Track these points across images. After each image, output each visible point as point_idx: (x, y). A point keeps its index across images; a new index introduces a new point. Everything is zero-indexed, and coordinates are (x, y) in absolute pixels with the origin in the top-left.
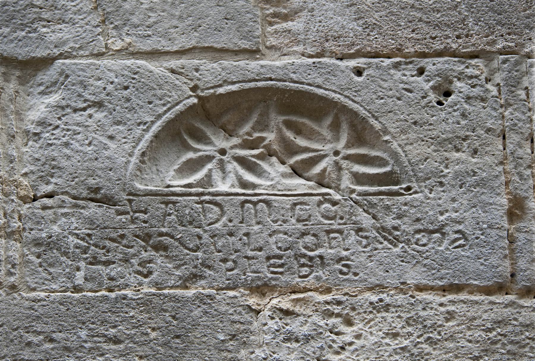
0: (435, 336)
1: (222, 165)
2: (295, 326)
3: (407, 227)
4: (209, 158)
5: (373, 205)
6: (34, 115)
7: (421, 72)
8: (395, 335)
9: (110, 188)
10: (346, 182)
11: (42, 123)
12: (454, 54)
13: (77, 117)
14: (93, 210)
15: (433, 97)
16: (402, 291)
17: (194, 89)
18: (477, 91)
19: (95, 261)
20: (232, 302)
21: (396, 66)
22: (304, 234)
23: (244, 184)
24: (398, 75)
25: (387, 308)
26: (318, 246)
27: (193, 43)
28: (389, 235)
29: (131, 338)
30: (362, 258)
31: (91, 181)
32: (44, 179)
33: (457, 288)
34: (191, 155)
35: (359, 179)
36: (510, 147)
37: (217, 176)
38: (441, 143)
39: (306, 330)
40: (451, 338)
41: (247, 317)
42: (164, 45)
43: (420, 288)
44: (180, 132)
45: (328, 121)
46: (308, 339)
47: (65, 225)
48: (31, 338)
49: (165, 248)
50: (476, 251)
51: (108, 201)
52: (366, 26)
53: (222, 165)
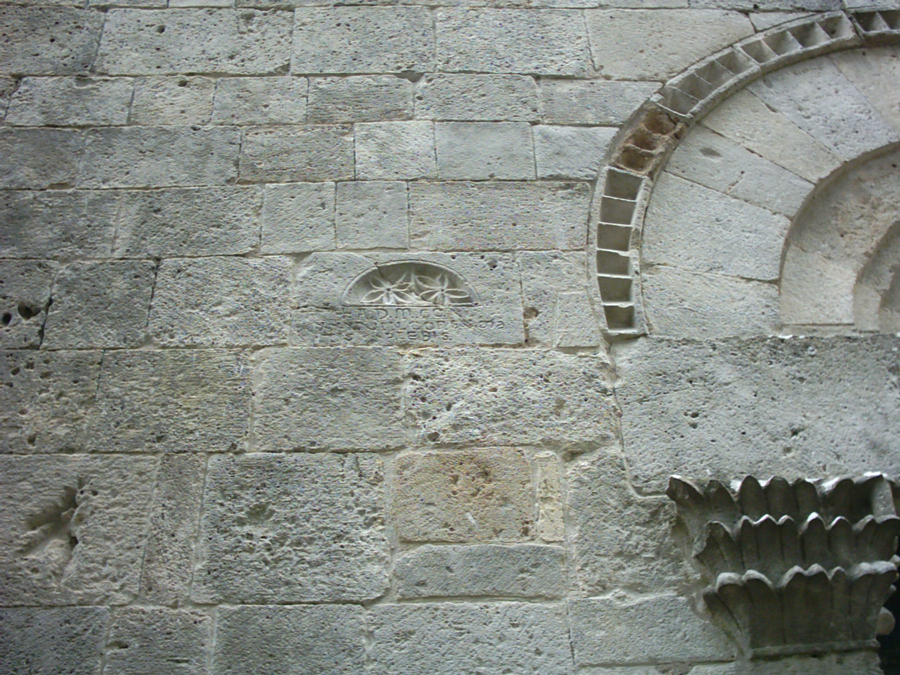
0: (489, 365)
1: (388, 295)
2: (420, 361)
3: (476, 319)
4: (382, 292)
5: (459, 311)
6: (301, 274)
7: (482, 257)
8: (469, 365)
9: (333, 302)
10: (447, 302)
11: (304, 277)
12: (497, 251)
13: (321, 275)
14: (325, 312)
15: (488, 267)
16: (473, 347)
17: (376, 263)
18: (508, 265)
19: (325, 334)
20: (390, 351)
21: (471, 255)
22: (426, 323)
23: (398, 303)
24: (471, 258)
25: (466, 353)
26: (432, 328)
27: (376, 245)
28: (467, 323)
29: (340, 366)
30: (454, 333)
31: (325, 301)
32: (303, 300)
33: (500, 345)
34: (373, 291)
35: (452, 300)
36: (524, 287)
37: (385, 299)
38: (491, 285)
39: (426, 363)
40: (497, 366)
41: (398, 357)
42: (363, 246)
43: (481, 346)
44: (370, 281)
45: (439, 277)
46: (426, 366)
47: (312, 318)
48: (292, 365)
49: (359, 329)
50: (508, 330)
51: (333, 309)
52: (457, 239)
53: (388, 295)
